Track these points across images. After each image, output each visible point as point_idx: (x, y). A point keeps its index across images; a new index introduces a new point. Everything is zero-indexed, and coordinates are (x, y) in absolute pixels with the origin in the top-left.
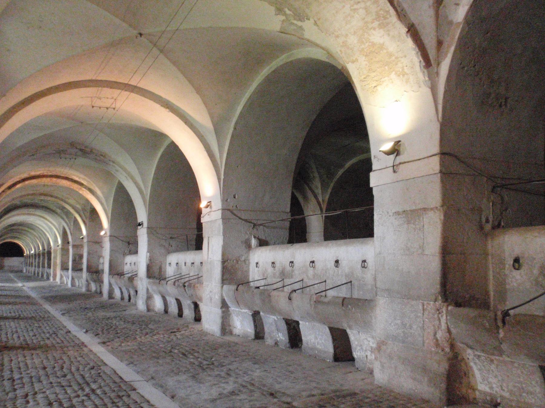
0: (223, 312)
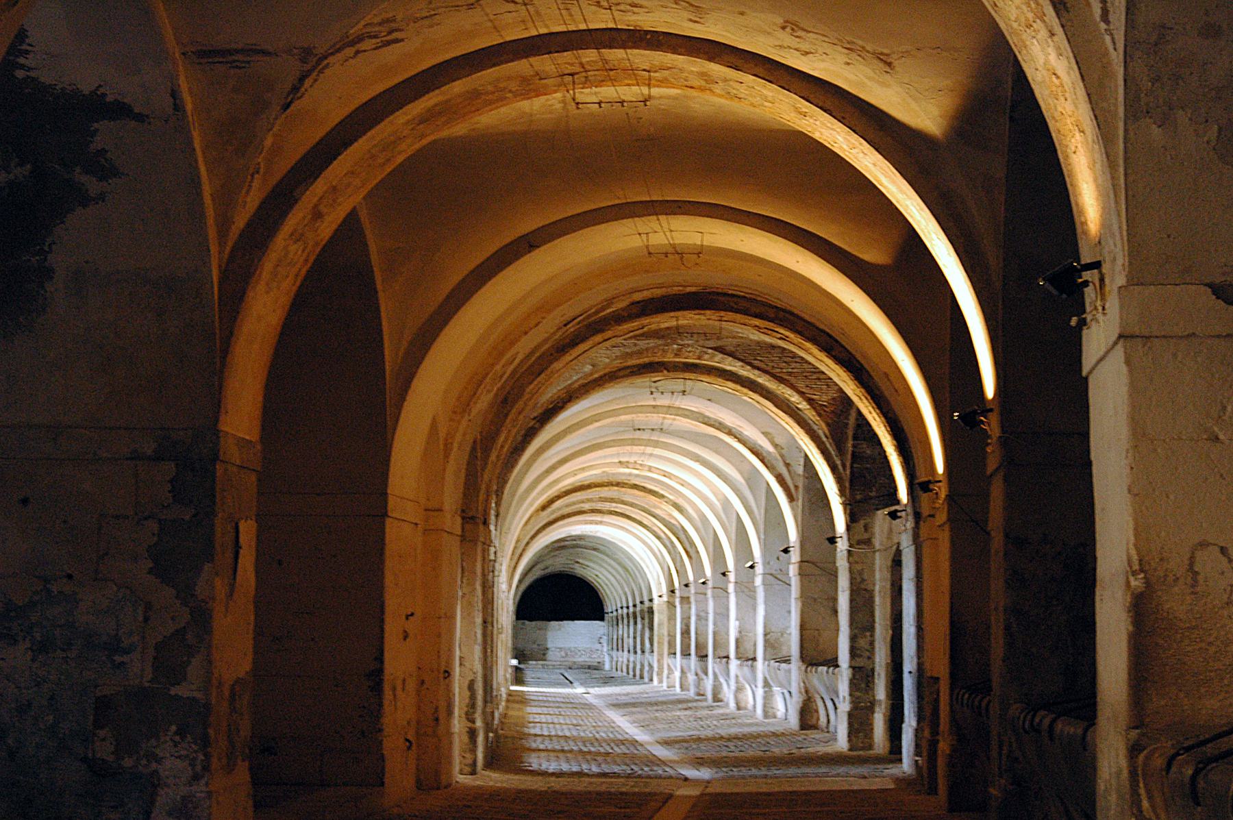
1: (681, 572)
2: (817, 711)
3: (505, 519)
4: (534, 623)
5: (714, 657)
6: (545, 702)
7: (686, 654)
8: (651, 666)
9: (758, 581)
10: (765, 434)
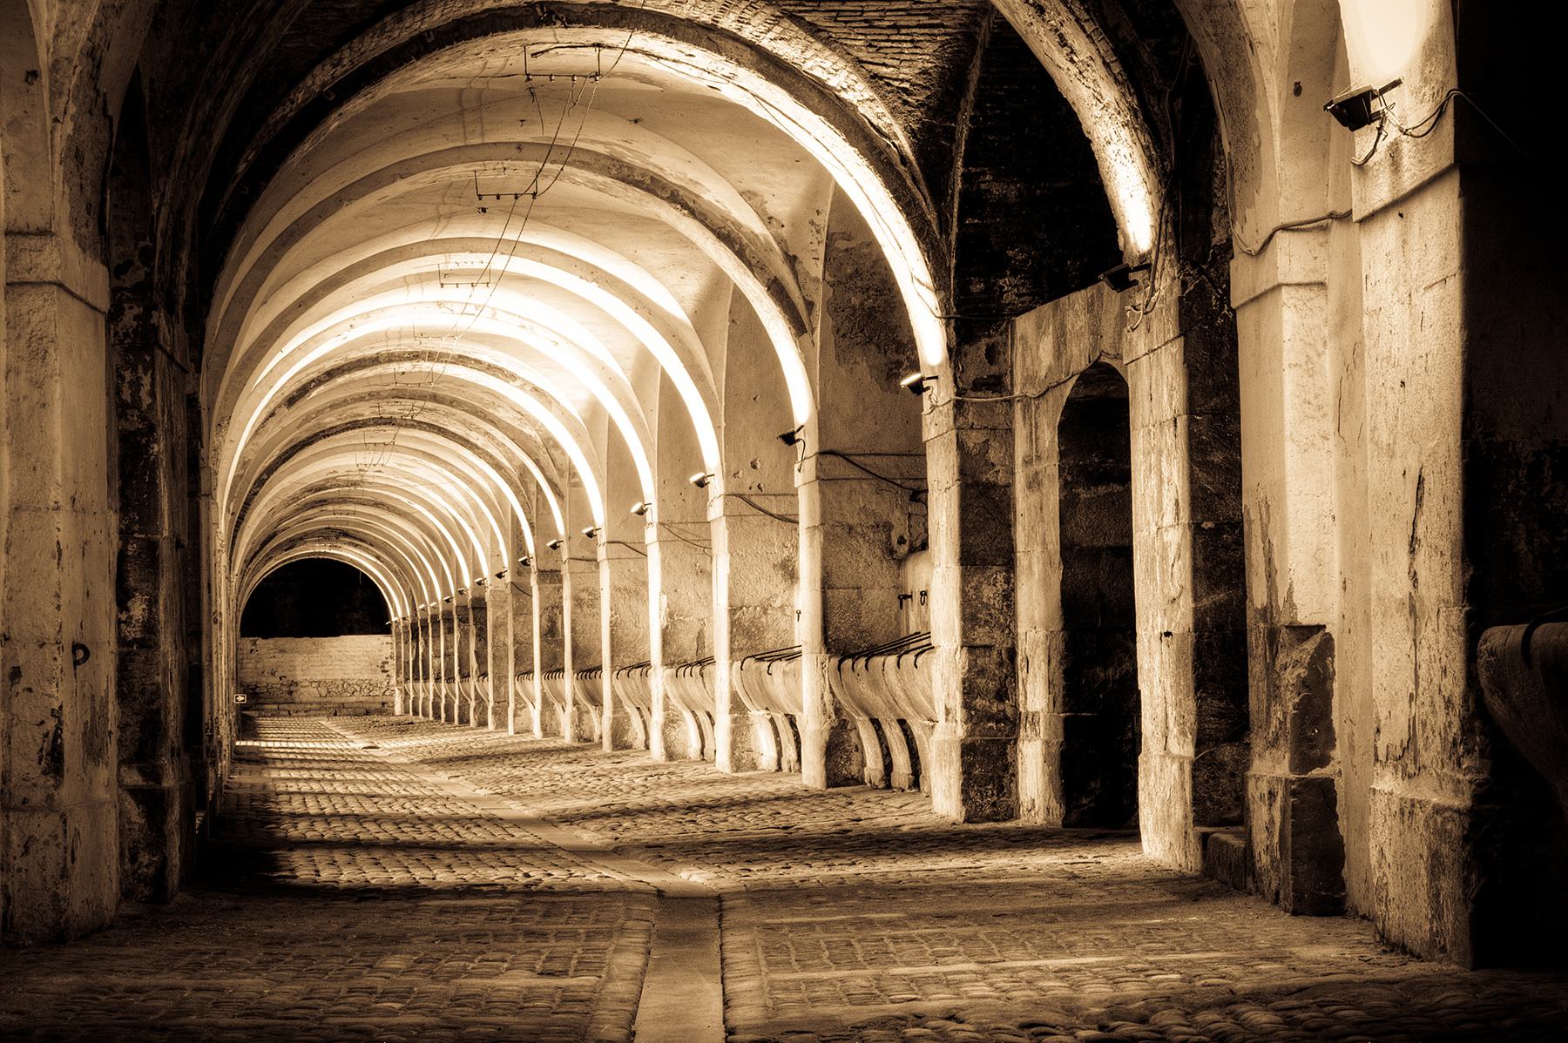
0: (735, 721)
1: (541, 525)
2: (859, 748)
4: (271, 641)
5: (613, 667)
6: (303, 762)
7: (552, 668)
8: (480, 701)
9: (716, 510)
10: (748, 195)
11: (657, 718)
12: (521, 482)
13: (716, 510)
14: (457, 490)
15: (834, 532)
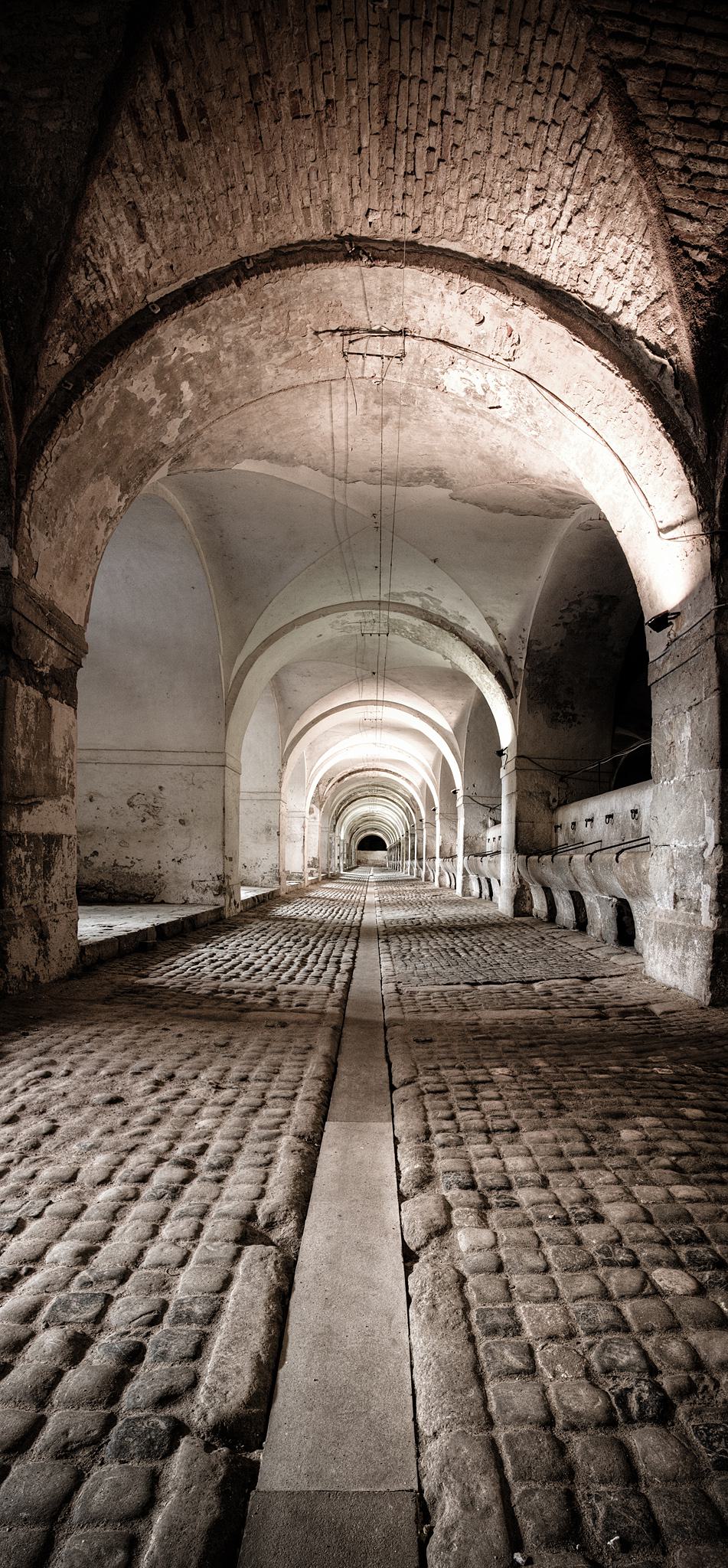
2: (530, 899)
3: (358, 761)
7: (413, 859)
9: (460, 802)
11: (437, 874)
12: (406, 811)
13: (460, 802)
14: (395, 816)
15: (522, 795)
